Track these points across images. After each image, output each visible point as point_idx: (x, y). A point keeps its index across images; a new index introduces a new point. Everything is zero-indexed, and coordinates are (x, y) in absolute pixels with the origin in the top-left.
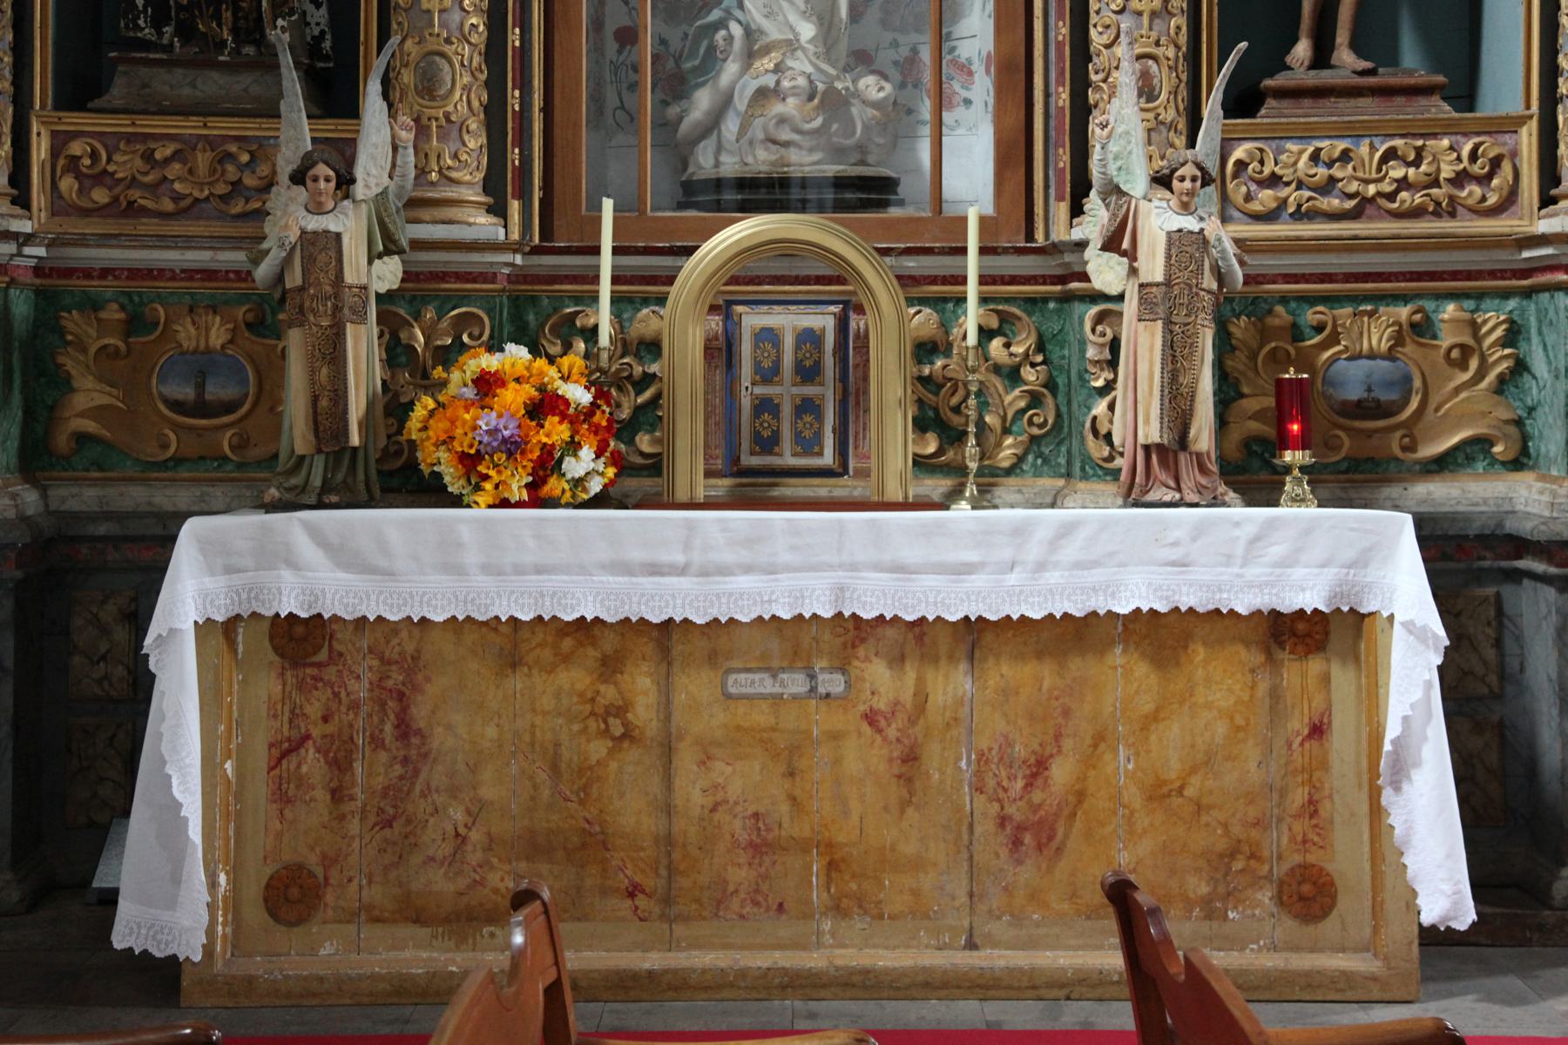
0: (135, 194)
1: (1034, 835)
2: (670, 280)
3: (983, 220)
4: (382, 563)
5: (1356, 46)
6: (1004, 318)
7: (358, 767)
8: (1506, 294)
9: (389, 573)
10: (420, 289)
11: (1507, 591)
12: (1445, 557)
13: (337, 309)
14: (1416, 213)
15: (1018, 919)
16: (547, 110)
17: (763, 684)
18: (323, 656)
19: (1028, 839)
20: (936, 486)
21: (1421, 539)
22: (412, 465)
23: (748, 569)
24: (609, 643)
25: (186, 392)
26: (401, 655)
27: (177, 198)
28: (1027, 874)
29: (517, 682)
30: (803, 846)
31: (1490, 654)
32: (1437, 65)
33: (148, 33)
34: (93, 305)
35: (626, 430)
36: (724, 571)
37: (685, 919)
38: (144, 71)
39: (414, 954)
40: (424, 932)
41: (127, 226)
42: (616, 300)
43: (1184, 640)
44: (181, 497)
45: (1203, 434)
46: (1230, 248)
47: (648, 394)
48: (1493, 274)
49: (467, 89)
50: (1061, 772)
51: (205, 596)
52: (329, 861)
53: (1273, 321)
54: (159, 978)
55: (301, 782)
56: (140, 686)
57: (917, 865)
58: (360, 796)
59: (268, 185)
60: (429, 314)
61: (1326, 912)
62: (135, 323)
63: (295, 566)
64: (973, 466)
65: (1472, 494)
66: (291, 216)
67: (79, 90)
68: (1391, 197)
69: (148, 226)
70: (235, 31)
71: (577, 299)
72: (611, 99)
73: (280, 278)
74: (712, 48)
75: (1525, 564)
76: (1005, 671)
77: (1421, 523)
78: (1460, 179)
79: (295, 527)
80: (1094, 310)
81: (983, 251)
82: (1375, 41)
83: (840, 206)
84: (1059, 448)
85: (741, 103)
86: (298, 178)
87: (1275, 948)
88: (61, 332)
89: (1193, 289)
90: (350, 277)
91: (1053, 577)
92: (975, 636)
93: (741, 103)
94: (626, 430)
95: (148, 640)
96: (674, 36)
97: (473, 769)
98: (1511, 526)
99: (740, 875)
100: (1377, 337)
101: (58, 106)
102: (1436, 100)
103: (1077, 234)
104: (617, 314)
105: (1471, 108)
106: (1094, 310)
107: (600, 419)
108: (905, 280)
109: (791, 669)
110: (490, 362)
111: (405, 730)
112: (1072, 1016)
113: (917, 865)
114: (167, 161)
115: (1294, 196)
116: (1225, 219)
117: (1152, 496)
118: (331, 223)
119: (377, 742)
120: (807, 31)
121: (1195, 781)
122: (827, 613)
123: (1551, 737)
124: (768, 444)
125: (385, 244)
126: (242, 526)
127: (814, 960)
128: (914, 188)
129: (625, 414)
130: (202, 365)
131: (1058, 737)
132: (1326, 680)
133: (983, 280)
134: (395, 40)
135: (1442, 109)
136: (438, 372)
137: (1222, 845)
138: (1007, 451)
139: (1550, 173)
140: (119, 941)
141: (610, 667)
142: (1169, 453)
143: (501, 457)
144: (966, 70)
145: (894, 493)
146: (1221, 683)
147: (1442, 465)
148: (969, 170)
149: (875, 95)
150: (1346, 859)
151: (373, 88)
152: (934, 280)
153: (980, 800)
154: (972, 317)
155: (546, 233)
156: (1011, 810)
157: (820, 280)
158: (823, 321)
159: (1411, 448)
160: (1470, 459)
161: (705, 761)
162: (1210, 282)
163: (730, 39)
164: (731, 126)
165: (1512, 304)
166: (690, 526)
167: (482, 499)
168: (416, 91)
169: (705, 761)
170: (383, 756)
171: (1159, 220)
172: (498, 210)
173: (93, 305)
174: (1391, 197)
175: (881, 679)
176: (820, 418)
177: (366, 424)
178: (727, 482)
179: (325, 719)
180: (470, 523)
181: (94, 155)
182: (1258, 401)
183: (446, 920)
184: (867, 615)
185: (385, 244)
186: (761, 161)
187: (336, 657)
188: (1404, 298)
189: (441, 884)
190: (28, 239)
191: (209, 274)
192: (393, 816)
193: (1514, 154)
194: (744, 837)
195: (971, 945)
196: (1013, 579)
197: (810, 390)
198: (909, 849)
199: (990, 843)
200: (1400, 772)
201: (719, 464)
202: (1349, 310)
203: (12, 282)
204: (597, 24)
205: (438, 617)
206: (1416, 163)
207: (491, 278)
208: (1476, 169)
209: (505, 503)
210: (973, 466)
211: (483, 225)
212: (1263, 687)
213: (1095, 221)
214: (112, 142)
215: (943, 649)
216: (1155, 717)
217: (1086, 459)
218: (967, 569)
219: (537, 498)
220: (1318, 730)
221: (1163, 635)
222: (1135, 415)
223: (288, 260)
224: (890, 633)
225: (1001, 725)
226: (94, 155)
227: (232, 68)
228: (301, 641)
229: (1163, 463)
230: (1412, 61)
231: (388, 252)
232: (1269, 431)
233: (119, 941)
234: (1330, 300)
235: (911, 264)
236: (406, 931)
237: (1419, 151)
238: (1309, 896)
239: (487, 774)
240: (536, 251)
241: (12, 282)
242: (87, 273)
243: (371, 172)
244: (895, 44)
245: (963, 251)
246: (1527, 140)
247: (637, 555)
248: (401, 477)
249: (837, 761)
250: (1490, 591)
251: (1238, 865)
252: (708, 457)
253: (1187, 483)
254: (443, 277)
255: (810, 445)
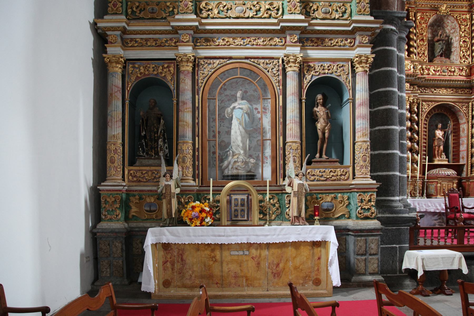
0: (140, 179)
1: (277, 275)
2: (221, 191)
3: (270, 181)
4: (178, 235)
5: (326, 155)
6: (273, 196)
7: (175, 265)
8: (347, 193)
9: (179, 237)
10: (183, 193)
11: (347, 237)
12: (338, 232)
13: (170, 196)
14: (335, 180)
15: (274, 287)
16: (202, 165)
17: (236, 253)
18: (170, 249)
19: (276, 275)
20: (262, 222)
21: (335, 230)
22: (182, 220)
23: (234, 236)
24: (213, 247)
25: (148, 209)
26: (181, 249)
27: (146, 179)
28: (276, 280)
29: (199, 253)
30: (242, 277)
31: (344, 246)
32: (338, 158)
33: (142, 154)
34: (134, 196)
35: (215, 214)
36: (230, 236)
37: (224, 287)
38: (141, 160)
39: (185, 292)
40: (186, 289)
41: (139, 184)
42: (213, 194)
43: (300, 245)
44: (148, 225)
45: (303, 214)
46: (307, 186)
47: (218, 209)
48: (346, 189)
49: (189, 162)
50: (281, 265)
51: (152, 240)
52: (172, 279)
53: (314, 197)
54: (148, 295)
55: (167, 267)
56: (143, 253)
57: (260, 279)
58: (176, 270)
59: (160, 177)
60: (184, 197)
61: (319, 285)
62: (141, 198)
63: (165, 236)
64: (268, 219)
65: (342, 223)
66: (163, 182)
67: (132, 163)
68: (331, 178)
69: (142, 184)
70: (155, 153)
71: (207, 194)
72: (212, 163)
73: (162, 192)
74: (227, 155)
75: (349, 233)
76: (273, 251)
77: (335, 227)
78: (341, 175)
79: (165, 229)
80: (287, 195)
81: (270, 186)
82: (328, 154)
83: (247, 179)
84: (281, 216)
85: (232, 163)
86: (164, 176)
87: (312, 290)
88: (130, 200)
89: (302, 192)
90: (172, 191)
91: (280, 236)
92: (268, 246)
93: (232, 163)
94: (215, 214)
95: (144, 246)
96: (221, 153)
97: (193, 266)
98: (348, 227)
99: (233, 281)
100: (329, 199)
101: (129, 166)
102: (338, 163)
103: (284, 184)
104: (213, 196)
105: (342, 164)
106: (287, 195)
107: (211, 213)
108: (258, 191)
109: (240, 251)
110: (194, 204)
111: (182, 260)
112: (282, 300)
113: (260, 279)
114: (145, 174)
115: (317, 178)
116: (306, 181)
117: (295, 224)
118: (169, 183)
119: (178, 262)
120: (242, 152)
121: (301, 266)
122: (246, 242)
123: (353, 258)
124: (236, 216)
125: (178, 186)
126: (157, 230)
127: (244, 293)
128: (259, 176)
129: (214, 212)
130: (150, 205)
131: (281, 260)
132: (321, 251)
133: (270, 191)
134: (179, 154)
135: (338, 164)
136: (186, 206)
137: (305, 275)
138: (273, 217)
139: (354, 174)
140: (142, 290)
141: (213, 250)
142: (298, 217)
143: (196, 219)
144: (267, 158)
145: (256, 224)
146: (305, 252)
147: (338, 218)
148: (267, 173)
149: (253, 162)
150: (323, 277)
151: (175, 162)
152: (262, 191)
153: (269, 270)
154: (268, 196)
155: (202, 184)
156: (274, 271)
157: (244, 191)
158: (245, 197)
159: (334, 216)
160: (342, 217)
161: (228, 264)
162: (304, 191)
163: (230, 153)
164: (230, 167)
165: (348, 194)
166: (225, 229)
167: (193, 225)
168: (182, 162)
169: (228, 264)
170: (179, 264)
171: (297, 182)
172: (194, 180)
173: (134, 196)
174: (331, 178)
175: (254, 252)
176: (244, 212)
177: (175, 214)
178: (230, 222)
179: (170, 258)
180: (191, 229)
181: (134, 173)
182: (311, 209)
183: (189, 287)
184: (252, 242)
185: (178, 186)
186: (235, 172)
187: (172, 249)
188: (333, 193)
189: (188, 282)
190: (125, 186)
191: (151, 191)
192: (181, 272)
193: (349, 171)
194: (233, 276)
195: (268, 291)
196: (274, 237)
197: (243, 208)
198: (258, 277)
199: (270, 276)
200: (331, 264)
201: (229, 219)
202: (325, 195)
203: (123, 193)
204: (209, 151)
205: (187, 243)
206: (335, 173)
207: (194, 191)
208: (343, 174)
209: (196, 226)
210: (268, 219)
211: (192, 183)
212: (311, 252)
213: (287, 182)
214: (137, 171)
215: (264, 248)
216: (295, 257)
217: (285, 218)
218: (267, 235)
219: (201, 225)
220: (319, 258)
221: (296, 245)
222: (293, 211)
223: (163, 189)
224: (256, 245)
225: (272, 259)
226: (134, 173)
227: (154, 159)
228: (166, 247)
229: (297, 219)
230: (334, 157)
231: (178, 187)
232: (313, 213)
233: (142, 290)
234: (322, 193)
235: (258, 188)
236: (183, 289)
237: (335, 171)
238: (317, 282)
239: (195, 266)
240: (200, 187)
241: (123, 193)
242: (133, 191)
243: (175, 175)
244: (256, 154)
245: (266, 186)
246: (351, 169)
247: (217, 234)
248: (180, 222)
249: (247, 264)
250: (344, 237)
251: (307, 278)
252: (227, 218)
253: (300, 222)
254: (186, 191)
255: (243, 216)
